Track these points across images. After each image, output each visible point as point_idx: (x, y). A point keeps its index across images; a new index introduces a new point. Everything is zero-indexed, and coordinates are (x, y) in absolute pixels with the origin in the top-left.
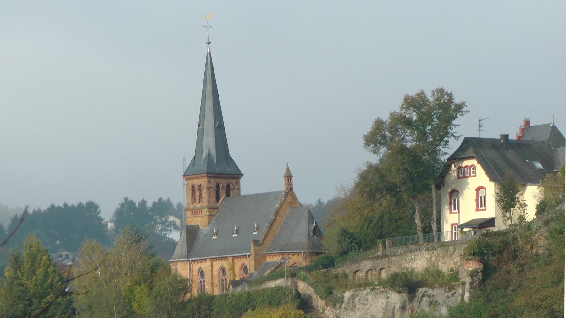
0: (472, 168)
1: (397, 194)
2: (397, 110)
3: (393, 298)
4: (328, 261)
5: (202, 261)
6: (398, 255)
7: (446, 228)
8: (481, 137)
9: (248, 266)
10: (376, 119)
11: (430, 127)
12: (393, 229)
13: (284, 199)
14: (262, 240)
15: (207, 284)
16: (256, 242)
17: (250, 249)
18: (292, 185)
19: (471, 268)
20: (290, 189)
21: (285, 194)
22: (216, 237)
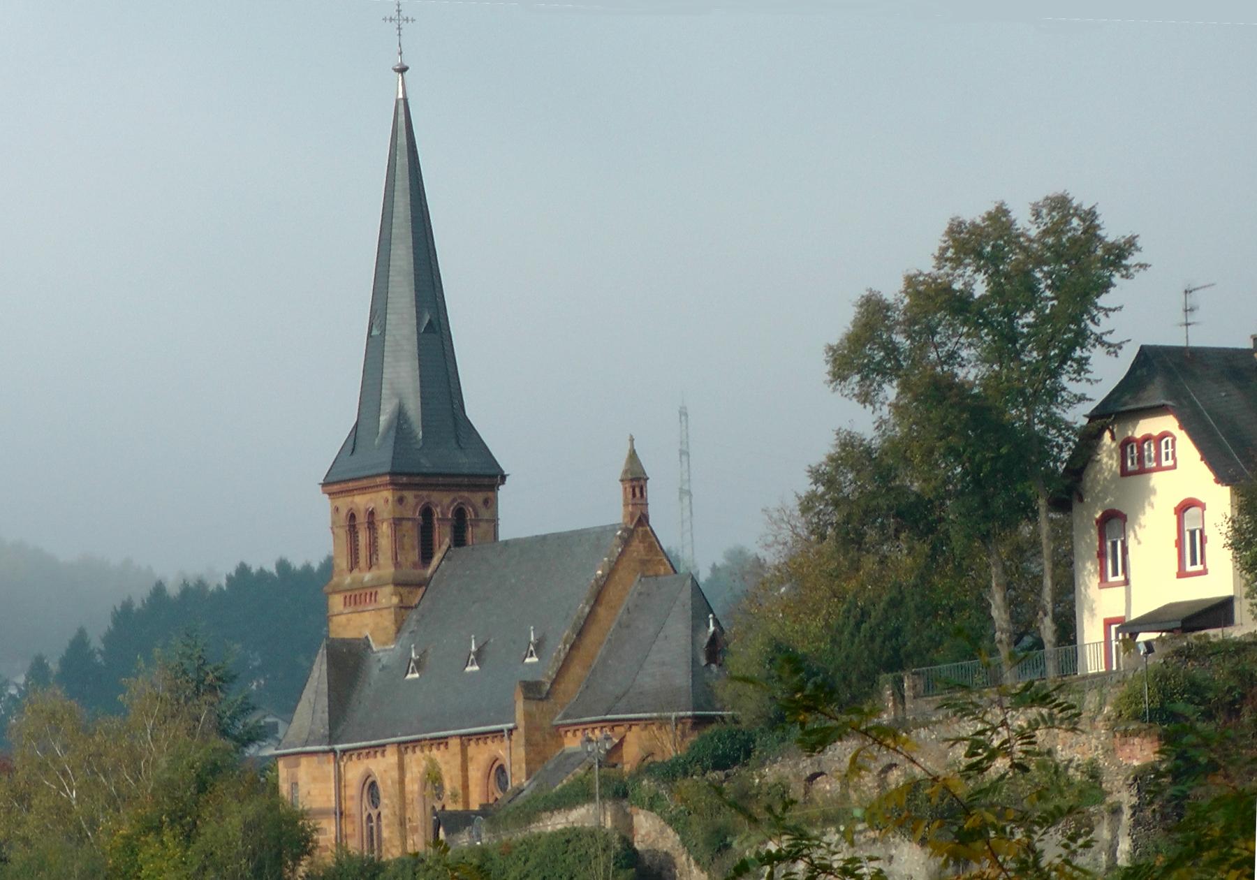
0: (1163, 443)
1: (931, 529)
2: (927, 266)
3: (906, 861)
4: (733, 744)
5: (372, 753)
6: (936, 723)
7: (1091, 633)
8: (1191, 345)
9: (508, 764)
10: (863, 297)
11: (1030, 318)
12: (931, 639)
13: (620, 550)
14: (550, 682)
15: (387, 826)
16: (532, 690)
17: (514, 712)
18: (647, 504)
19: (1138, 759)
20: (640, 518)
21: (625, 535)
22: (417, 675)
